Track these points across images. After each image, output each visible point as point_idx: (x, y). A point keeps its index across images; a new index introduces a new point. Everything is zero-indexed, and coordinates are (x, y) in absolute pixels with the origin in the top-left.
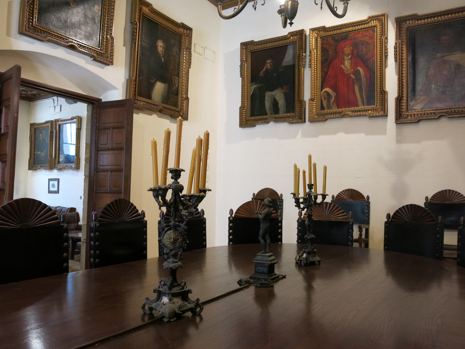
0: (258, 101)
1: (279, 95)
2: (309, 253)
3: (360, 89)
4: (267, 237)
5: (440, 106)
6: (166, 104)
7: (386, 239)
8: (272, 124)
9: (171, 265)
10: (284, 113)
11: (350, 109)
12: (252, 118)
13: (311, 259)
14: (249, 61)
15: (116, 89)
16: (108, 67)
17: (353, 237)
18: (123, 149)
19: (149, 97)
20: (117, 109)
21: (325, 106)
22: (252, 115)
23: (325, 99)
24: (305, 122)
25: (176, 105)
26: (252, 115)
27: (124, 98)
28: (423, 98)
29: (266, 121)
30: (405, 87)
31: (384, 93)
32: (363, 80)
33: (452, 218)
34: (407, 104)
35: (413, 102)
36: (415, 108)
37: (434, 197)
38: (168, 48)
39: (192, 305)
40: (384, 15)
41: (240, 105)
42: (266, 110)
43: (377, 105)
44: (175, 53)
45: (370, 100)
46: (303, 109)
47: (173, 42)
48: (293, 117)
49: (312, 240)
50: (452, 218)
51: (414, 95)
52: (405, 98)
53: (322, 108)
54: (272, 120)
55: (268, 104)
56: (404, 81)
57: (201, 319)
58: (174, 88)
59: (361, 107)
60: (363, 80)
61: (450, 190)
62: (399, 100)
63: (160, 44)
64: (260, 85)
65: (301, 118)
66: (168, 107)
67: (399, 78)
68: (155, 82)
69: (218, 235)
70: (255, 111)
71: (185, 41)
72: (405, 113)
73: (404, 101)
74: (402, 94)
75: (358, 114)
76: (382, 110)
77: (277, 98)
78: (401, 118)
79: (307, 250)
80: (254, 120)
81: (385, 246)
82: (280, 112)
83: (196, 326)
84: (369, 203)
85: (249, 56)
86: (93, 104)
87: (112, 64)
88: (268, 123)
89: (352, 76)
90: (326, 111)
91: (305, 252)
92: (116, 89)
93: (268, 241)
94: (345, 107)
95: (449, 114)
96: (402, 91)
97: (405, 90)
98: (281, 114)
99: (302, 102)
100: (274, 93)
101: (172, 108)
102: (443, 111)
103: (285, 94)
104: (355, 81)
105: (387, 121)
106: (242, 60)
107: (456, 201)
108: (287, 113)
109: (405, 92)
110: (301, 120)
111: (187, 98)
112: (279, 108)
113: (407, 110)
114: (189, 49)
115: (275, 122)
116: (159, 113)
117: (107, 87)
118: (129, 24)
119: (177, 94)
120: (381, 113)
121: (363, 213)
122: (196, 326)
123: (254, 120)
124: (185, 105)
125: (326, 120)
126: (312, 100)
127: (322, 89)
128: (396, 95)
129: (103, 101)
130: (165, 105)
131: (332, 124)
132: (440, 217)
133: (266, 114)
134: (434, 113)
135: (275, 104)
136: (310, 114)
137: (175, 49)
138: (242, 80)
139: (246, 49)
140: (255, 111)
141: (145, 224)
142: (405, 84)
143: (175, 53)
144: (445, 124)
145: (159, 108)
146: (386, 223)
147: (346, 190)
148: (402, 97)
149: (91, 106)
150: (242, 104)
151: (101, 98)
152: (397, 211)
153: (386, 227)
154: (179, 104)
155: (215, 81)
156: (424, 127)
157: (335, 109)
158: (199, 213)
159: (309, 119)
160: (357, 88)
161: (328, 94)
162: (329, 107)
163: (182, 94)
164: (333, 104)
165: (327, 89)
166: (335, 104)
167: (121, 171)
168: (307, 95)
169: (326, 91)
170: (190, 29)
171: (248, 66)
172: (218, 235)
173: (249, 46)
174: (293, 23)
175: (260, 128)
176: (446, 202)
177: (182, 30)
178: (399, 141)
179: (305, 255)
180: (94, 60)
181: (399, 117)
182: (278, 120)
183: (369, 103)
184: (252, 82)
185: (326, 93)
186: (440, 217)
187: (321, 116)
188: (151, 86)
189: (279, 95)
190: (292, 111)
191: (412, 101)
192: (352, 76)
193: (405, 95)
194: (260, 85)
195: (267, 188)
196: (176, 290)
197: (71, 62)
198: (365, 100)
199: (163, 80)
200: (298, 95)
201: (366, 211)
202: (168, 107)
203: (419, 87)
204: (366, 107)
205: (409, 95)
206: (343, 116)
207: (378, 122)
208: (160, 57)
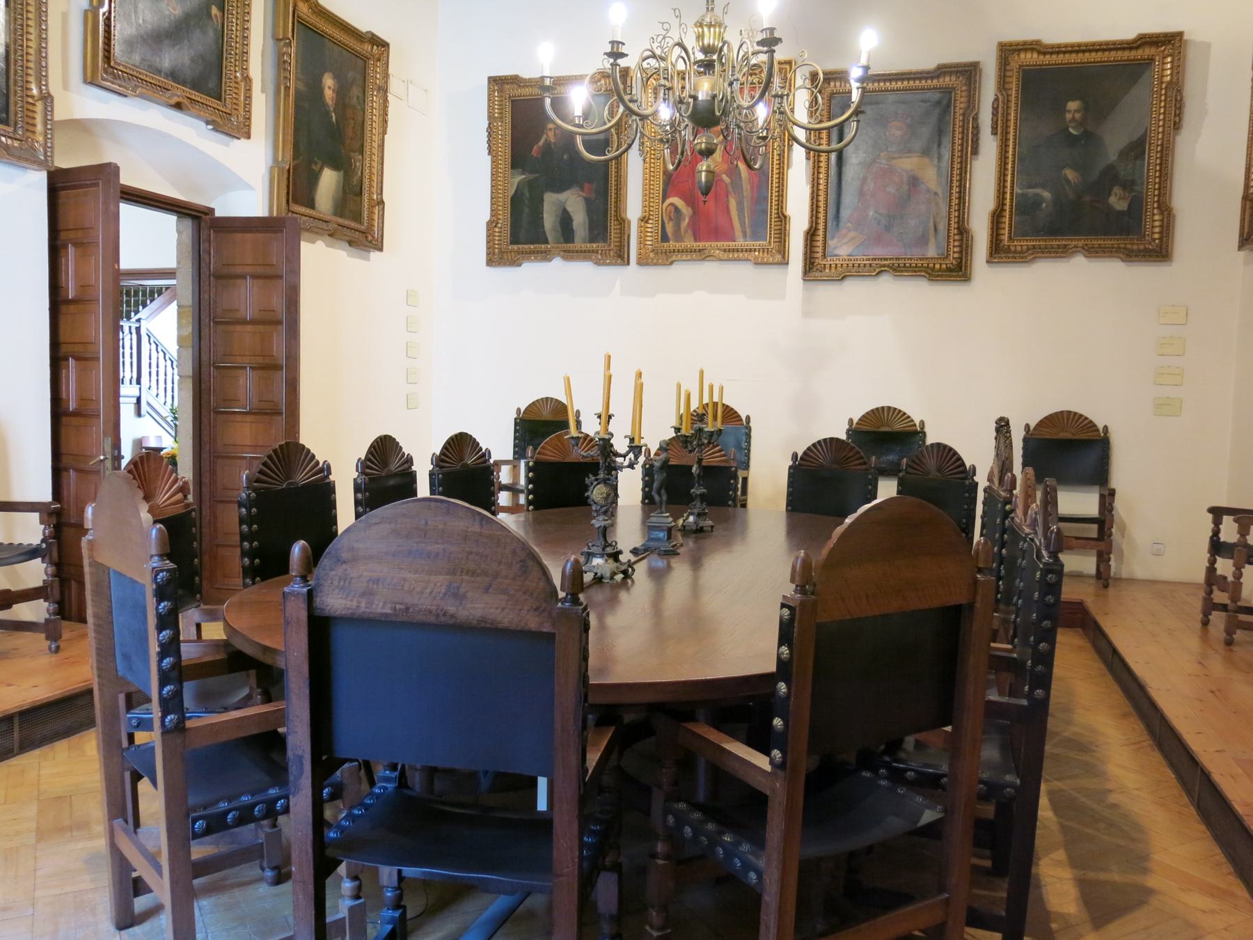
0: (526, 210)
1: (574, 202)
2: (699, 515)
3: (740, 204)
4: (663, 491)
5: (879, 251)
6: (341, 216)
7: (789, 494)
8: (557, 262)
9: (603, 524)
10: (584, 242)
12: (515, 247)
13: (702, 524)
14: (508, 120)
15: (250, 188)
16: (236, 141)
18: (281, 323)
19: (311, 204)
20: (260, 236)
21: (670, 235)
22: (515, 240)
23: (670, 219)
24: (628, 264)
25: (357, 217)
26: (515, 240)
28: (852, 234)
29: (546, 256)
30: (821, 210)
31: (783, 219)
32: (746, 186)
33: (891, 457)
35: (835, 240)
36: (837, 252)
37: (864, 418)
38: (342, 92)
39: (623, 568)
40: (789, 63)
41: (488, 217)
42: (544, 232)
43: (769, 241)
44: (354, 100)
45: (757, 231)
47: (350, 74)
48: (605, 254)
49: (702, 496)
50: (891, 457)
51: (838, 225)
52: (821, 232)
53: (665, 238)
54: (558, 255)
55: (549, 220)
56: (821, 198)
57: (633, 582)
58: (355, 180)
59: (740, 242)
60: (746, 186)
61: (889, 408)
62: (811, 235)
63: (328, 82)
64: (531, 176)
65: (620, 256)
66: (346, 222)
67: (813, 193)
68: (321, 169)
70: (521, 231)
71: (375, 73)
72: (819, 261)
74: (817, 224)
75: (734, 255)
76: (779, 252)
77: (569, 209)
78: (811, 267)
79: (696, 511)
80: (518, 252)
81: (788, 505)
82: (576, 240)
83: (628, 589)
84: (749, 429)
85: (508, 109)
86: (194, 218)
87: (249, 137)
88: (550, 260)
89: (724, 177)
90: (672, 244)
91: (691, 514)
92: (250, 188)
93: (664, 498)
94: (709, 240)
95: (895, 270)
96: (817, 218)
97: (821, 216)
98: (579, 244)
99: (623, 223)
100: (563, 196)
101: (353, 224)
103: (588, 201)
104: (730, 189)
106: (491, 117)
107: (898, 426)
108: (591, 241)
109: (821, 221)
110: (621, 257)
111: (381, 203)
112: (572, 231)
113: (824, 256)
114: (384, 90)
115: (565, 258)
116: (328, 238)
117: (232, 182)
118: (270, 42)
119: (361, 193)
120: (778, 257)
121: (739, 448)
122: (628, 589)
123: (518, 252)
125: (671, 263)
126: (644, 220)
127: (664, 198)
128: (805, 225)
129: (218, 214)
130: (340, 221)
131: (684, 271)
132: (873, 458)
133: (546, 242)
135: (565, 221)
137: (355, 91)
138: (493, 162)
139: (500, 91)
140: (521, 231)
142: (821, 204)
143: (354, 100)
144: (887, 285)
145: (331, 226)
146: (790, 467)
147: (825, 440)
148: (816, 229)
150: (492, 216)
152: (809, 449)
153: (790, 475)
154: (365, 214)
155: (436, 164)
156: (855, 289)
157: (689, 243)
158: (965, 471)
160: (733, 204)
161: (677, 209)
162: (678, 238)
163: (371, 193)
164: (686, 231)
165: (675, 200)
166: (690, 232)
167: (277, 367)
168: (633, 208)
169: (672, 204)
170: (384, 45)
171: (505, 130)
173: (507, 87)
174: (610, 55)
175: (531, 270)
176: (882, 429)
177: (367, 47)
178: (807, 314)
179: (691, 519)
180: (215, 129)
182: (570, 255)
183: (755, 236)
184: (513, 167)
185: (672, 208)
186: (873, 458)
187: (662, 252)
188: (314, 179)
189: (574, 202)
190: (601, 236)
191: (833, 238)
192: (724, 177)
193: (821, 227)
194: (531, 176)
195: (547, 399)
196: (609, 550)
197: (170, 136)
198: (748, 231)
199: (336, 167)
200: (616, 207)
201: (744, 445)
202: (346, 222)
203: (845, 213)
204: (750, 244)
205: (829, 225)
206: (702, 255)
207: (772, 273)
208: (327, 113)
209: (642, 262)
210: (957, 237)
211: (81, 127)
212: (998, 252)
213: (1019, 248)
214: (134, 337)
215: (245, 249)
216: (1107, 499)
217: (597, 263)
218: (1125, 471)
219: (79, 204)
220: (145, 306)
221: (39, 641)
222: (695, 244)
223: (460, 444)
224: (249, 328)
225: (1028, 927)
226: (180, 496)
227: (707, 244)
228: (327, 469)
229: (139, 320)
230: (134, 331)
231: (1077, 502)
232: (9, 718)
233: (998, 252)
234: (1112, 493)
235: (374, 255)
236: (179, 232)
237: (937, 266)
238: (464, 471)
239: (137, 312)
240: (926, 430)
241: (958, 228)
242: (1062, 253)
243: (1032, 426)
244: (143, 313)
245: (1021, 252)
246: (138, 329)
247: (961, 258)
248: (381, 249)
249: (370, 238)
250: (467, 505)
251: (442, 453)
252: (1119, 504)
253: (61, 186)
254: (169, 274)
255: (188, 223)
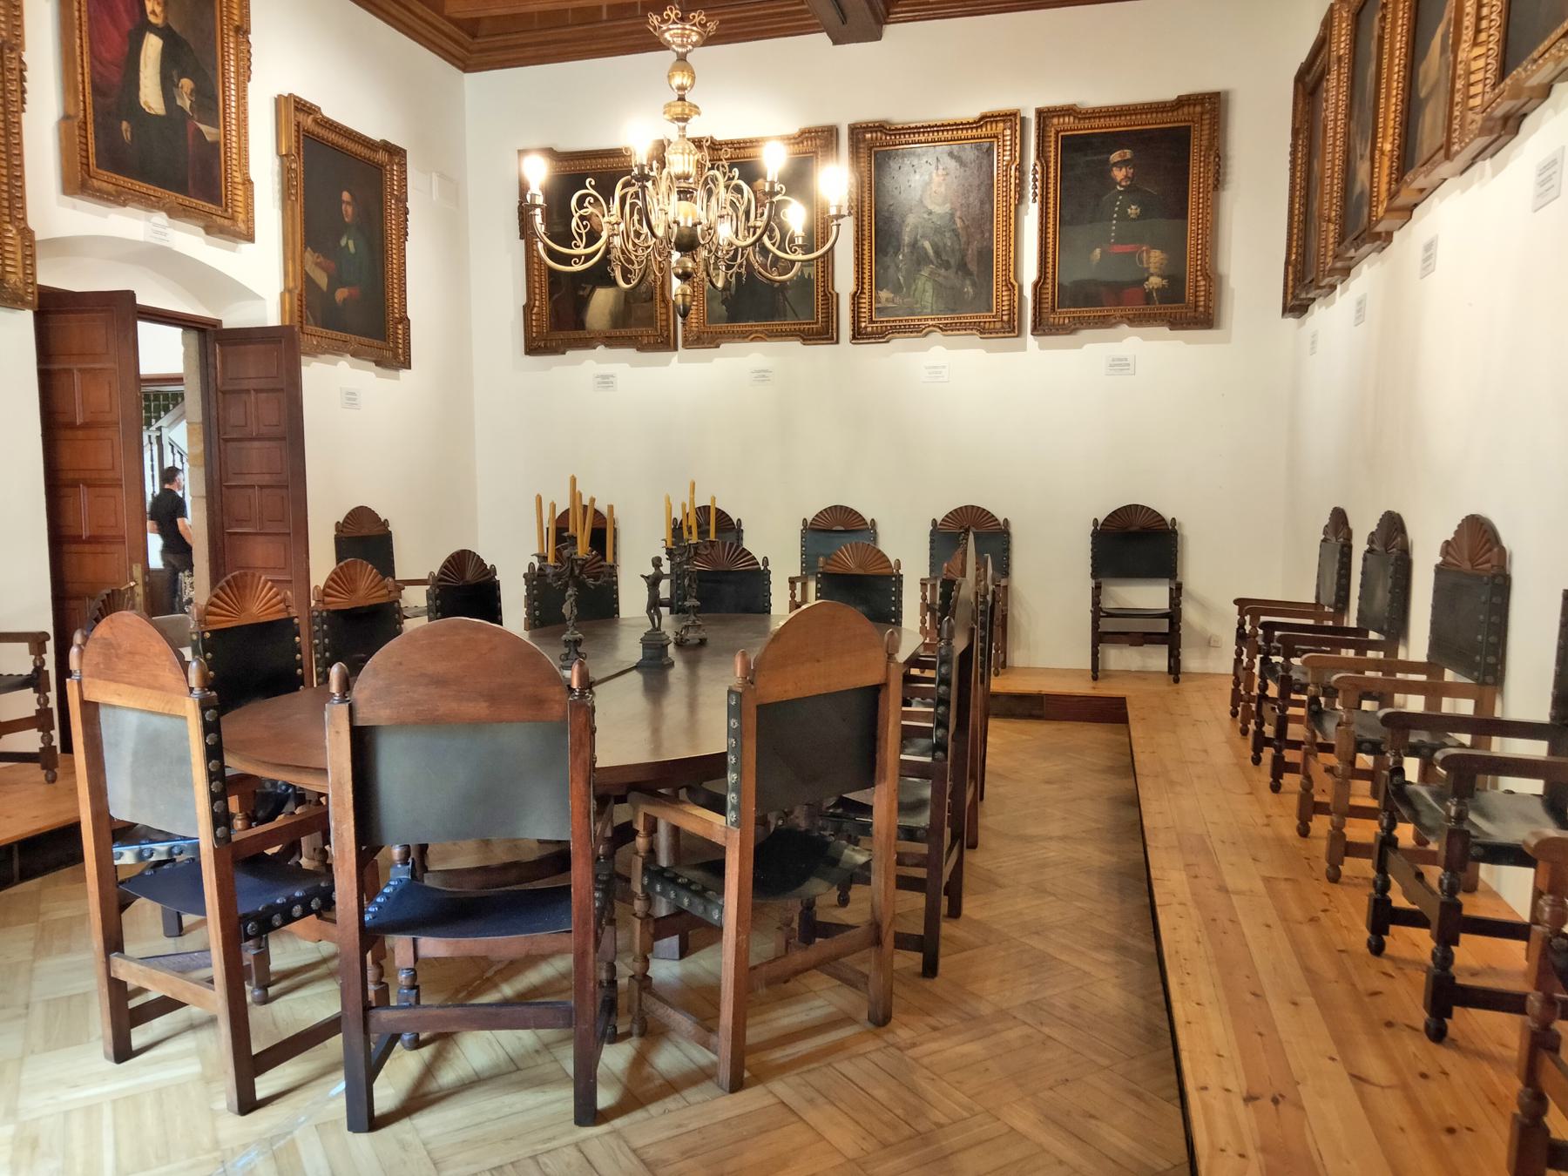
117: (240, 292)
129: (225, 326)
211: (62, 246)
214: (155, 448)
215: (252, 368)
216: (1176, 593)
218: (1197, 567)
219: (79, 333)
220: (167, 410)
221: (35, 771)
223: (461, 561)
224: (256, 444)
226: (282, 606)
228: (493, 570)
229: (159, 429)
230: (154, 440)
232: (8, 849)
236: (184, 344)
238: (466, 589)
239: (158, 418)
243: (1100, 521)
244: (163, 422)
246: (159, 439)
251: (441, 572)
253: (52, 310)
254: (177, 380)
255: (193, 335)
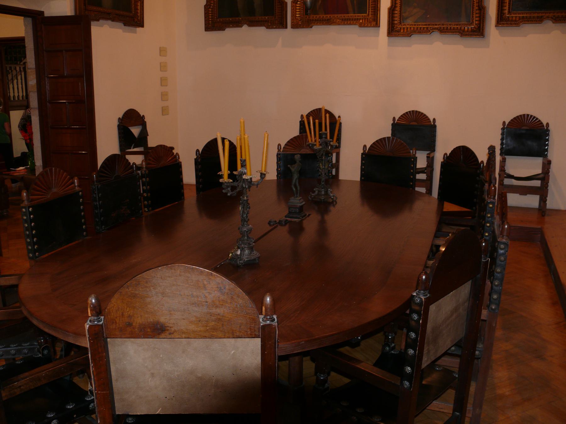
11: (339, 15)
17: (416, 166)
24: (286, 28)
27: (73, 14)
29: (238, 24)
34: (400, 15)
43: (370, 11)
46: (284, 12)
62: (391, 11)
69: (350, 168)
73: (397, 12)
78: (392, 31)
102: (436, 26)
105: (379, 30)
110: (282, 25)
124: (139, 7)
129: (46, 14)
134: (427, 28)
136: (292, 20)
141: (178, 166)
148: (395, 7)
149: (30, 20)
151: (42, 10)
153: (363, 159)
159: (292, 23)
172: (350, 168)
175: (230, 33)
181: (392, 30)
182: (252, 24)
193: (398, 5)
209: (294, 26)
210: (477, 12)
212: (501, 20)
213: (514, 18)
216: (547, 165)
217: (268, 27)
222: (325, 16)
225: (195, 188)
227: (332, 16)
231: (523, 167)
233: (501, 20)
234: (549, 162)
235: (139, 29)
237: (466, 28)
240: (437, 124)
241: (478, 6)
242: (539, 20)
245: (516, 21)
247: (480, 24)
248: (143, 26)
249: (136, 20)
250: (163, 208)
252: (554, 168)
